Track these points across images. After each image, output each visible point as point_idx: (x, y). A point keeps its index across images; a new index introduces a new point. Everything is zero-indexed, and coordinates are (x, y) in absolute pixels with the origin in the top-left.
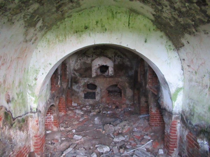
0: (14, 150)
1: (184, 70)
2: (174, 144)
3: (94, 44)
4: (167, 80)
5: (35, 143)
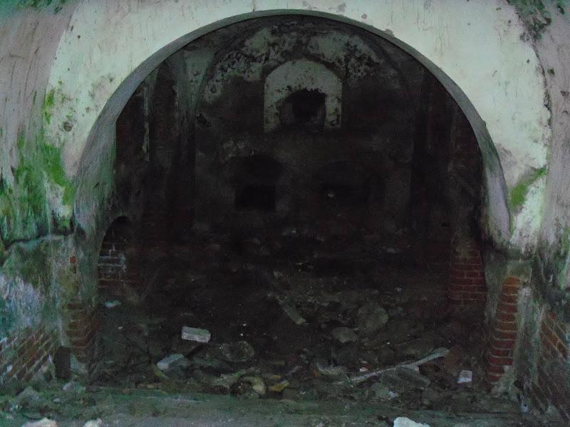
0: (10, 331)
1: (553, 109)
2: (506, 353)
3: (251, 11)
4: (495, 141)
5: (71, 326)
